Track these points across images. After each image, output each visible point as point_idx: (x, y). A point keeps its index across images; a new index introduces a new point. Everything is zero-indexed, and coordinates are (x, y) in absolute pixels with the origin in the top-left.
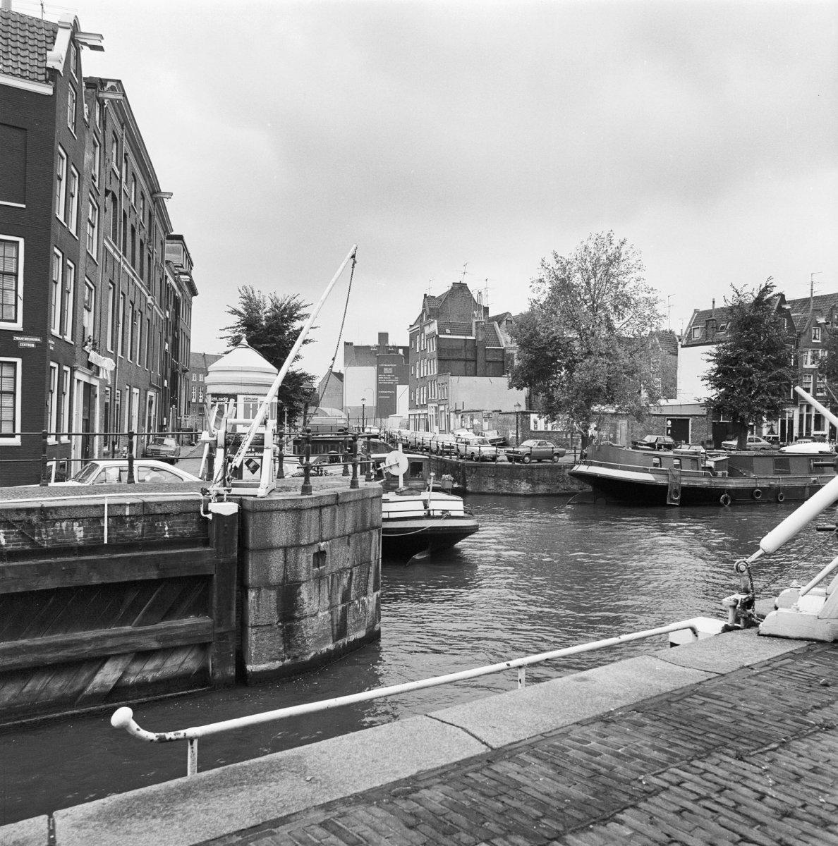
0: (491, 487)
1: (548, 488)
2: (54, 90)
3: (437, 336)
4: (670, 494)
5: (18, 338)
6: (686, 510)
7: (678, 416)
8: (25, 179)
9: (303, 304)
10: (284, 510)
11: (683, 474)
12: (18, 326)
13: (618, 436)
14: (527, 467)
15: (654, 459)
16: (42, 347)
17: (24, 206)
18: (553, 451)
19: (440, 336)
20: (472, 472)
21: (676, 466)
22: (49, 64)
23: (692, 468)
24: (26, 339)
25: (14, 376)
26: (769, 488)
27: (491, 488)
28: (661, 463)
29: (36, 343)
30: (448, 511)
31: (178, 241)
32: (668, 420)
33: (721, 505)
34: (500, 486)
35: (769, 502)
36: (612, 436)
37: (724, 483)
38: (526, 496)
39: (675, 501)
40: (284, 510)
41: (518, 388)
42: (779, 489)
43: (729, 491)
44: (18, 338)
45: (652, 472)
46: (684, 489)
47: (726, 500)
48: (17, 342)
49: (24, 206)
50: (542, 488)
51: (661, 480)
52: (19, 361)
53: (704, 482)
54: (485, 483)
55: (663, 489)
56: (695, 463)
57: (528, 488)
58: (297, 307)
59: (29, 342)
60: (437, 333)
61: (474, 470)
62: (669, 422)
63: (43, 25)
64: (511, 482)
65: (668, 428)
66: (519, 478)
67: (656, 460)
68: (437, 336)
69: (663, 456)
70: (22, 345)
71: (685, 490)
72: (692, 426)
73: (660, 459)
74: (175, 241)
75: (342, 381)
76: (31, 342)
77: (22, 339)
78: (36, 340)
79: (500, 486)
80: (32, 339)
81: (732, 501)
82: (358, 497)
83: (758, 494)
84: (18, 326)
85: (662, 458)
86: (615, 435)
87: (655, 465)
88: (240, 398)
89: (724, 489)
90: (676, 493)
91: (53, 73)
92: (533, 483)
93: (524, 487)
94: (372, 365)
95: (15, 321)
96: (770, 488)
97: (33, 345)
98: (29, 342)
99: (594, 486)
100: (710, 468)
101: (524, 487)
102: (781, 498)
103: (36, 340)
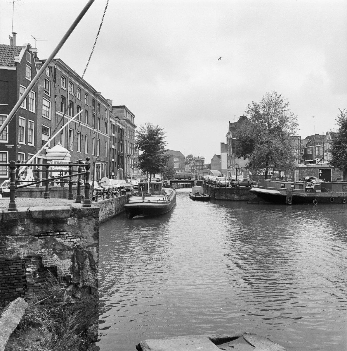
0: (224, 197)
1: (246, 197)
2: (16, 68)
3: (232, 138)
4: (287, 199)
5: (7, 145)
6: (297, 206)
7: (325, 168)
8: (8, 97)
9: (161, 129)
10: (26, 191)
11: (296, 191)
12: (7, 141)
13: (295, 177)
14: (237, 189)
15: (291, 185)
16: (15, 148)
17: (8, 105)
18: (249, 182)
19: (233, 138)
20: (217, 191)
21: (292, 188)
22: (15, 61)
23: (300, 189)
24: (10, 145)
25: (3, 157)
26: (338, 197)
27: (224, 197)
28: (294, 187)
29: (12, 146)
30: (150, 200)
31: (123, 108)
32: (320, 170)
33: (313, 204)
34: (227, 197)
35: (338, 203)
36: (292, 177)
37: (315, 195)
38: (236, 201)
39: (290, 202)
40: (26, 191)
41: (238, 158)
42: (343, 198)
43: (317, 198)
44: (7, 145)
45: (279, 190)
46: (294, 197)
47: (315, 202)
48: (7, 146)
49: (8, 105)
50: (243, 198)
51: (284, 194)
52: (7, 152)
53: (305, 194)
54: (222, 195)
55: (285, 197)
56: (302, 187)
57: (237, 197)
58: (158, 130)
59: (10, 146)
60: (232, 137)
61: (218, 190)
62: (321, 171)
63: (18, 48)
64: (231, 195)
65: (320, 174)
66: (234, 193)
67: (283, 185)
68: (232, 138)
69: (286, 183)
70: (8, 147)
71: (294, 198)
72: (332, 172)
73: (284, 185)
74: (122, 108)
75: (220, 159)
76: (11, 146)
77: (8, 145)
78: (13, 145)
79: (227, 197)
80: (11, 145)
81: (318, 203)
82: (63, 189)
83: (332, 200)
84: (7, 141)
85: (285, 184)
86: (293, 177)
87: (282, 187)
88: (53, 161)
89: (315, 197)
90: (290, 199)
91: (16, 63)
92: (240, 196)
93: (236, 197)
94: (225, 152)
95: (6, 140)
96: (339, 197)
97: (11, 147)
98: (10, 146)
99: (258, 196)
100: (312, 189)
101: (236, 197)
102: (344, 201)
103: (13, 145)
